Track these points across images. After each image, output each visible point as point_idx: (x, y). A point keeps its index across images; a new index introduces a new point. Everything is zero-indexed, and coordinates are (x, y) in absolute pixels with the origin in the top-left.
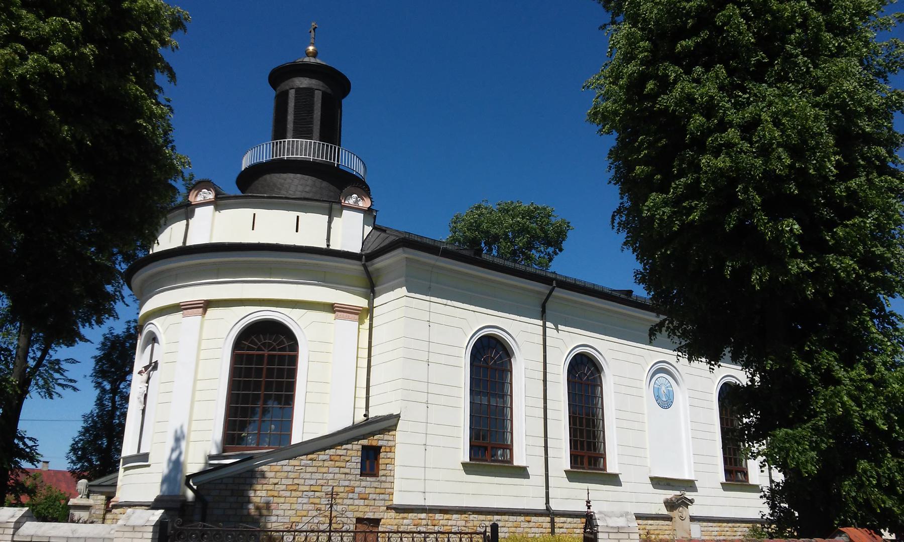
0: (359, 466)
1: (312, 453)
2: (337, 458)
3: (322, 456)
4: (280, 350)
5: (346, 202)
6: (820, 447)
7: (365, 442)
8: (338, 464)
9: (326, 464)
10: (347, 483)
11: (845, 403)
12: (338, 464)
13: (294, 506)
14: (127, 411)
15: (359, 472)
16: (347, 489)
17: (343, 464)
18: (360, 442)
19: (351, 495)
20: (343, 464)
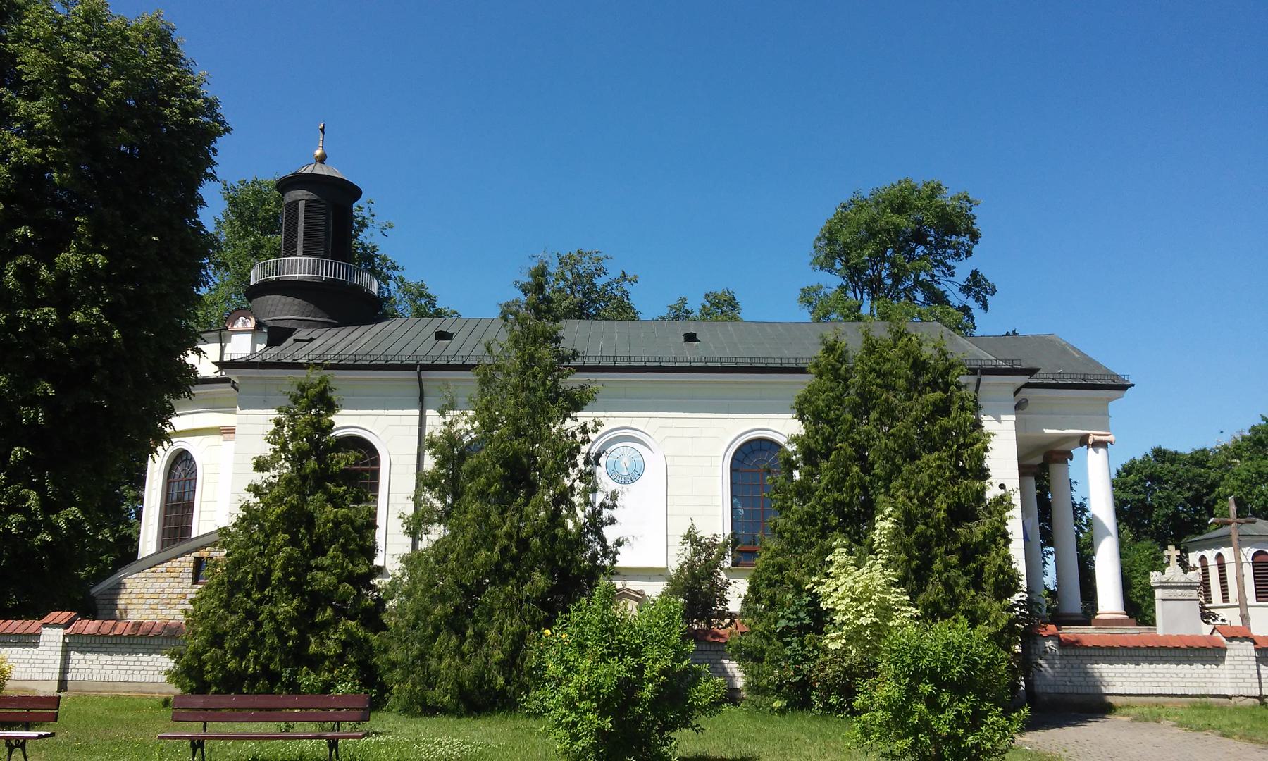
0: (191, 575)
1: (154, 566)
2: (172, 570)
3: (161, 568)
4: (362, 465)
5: (235, 326)
6: (892, 286)
7: (197, 554)
8: (172, 575)
9: (164, 575)
10: (179, 591)
11: (503, 584)
12: (172, 575)
13: (140, 611)
14: (376, 509)
15: (190, 580)
16: (179, 596)
17: (177, 575)
18: (193, 554)
19: (182, 601)
20: (177, 575)
